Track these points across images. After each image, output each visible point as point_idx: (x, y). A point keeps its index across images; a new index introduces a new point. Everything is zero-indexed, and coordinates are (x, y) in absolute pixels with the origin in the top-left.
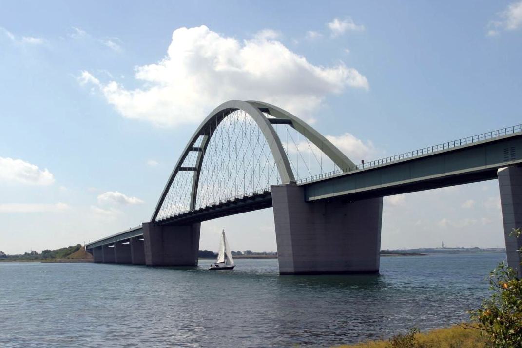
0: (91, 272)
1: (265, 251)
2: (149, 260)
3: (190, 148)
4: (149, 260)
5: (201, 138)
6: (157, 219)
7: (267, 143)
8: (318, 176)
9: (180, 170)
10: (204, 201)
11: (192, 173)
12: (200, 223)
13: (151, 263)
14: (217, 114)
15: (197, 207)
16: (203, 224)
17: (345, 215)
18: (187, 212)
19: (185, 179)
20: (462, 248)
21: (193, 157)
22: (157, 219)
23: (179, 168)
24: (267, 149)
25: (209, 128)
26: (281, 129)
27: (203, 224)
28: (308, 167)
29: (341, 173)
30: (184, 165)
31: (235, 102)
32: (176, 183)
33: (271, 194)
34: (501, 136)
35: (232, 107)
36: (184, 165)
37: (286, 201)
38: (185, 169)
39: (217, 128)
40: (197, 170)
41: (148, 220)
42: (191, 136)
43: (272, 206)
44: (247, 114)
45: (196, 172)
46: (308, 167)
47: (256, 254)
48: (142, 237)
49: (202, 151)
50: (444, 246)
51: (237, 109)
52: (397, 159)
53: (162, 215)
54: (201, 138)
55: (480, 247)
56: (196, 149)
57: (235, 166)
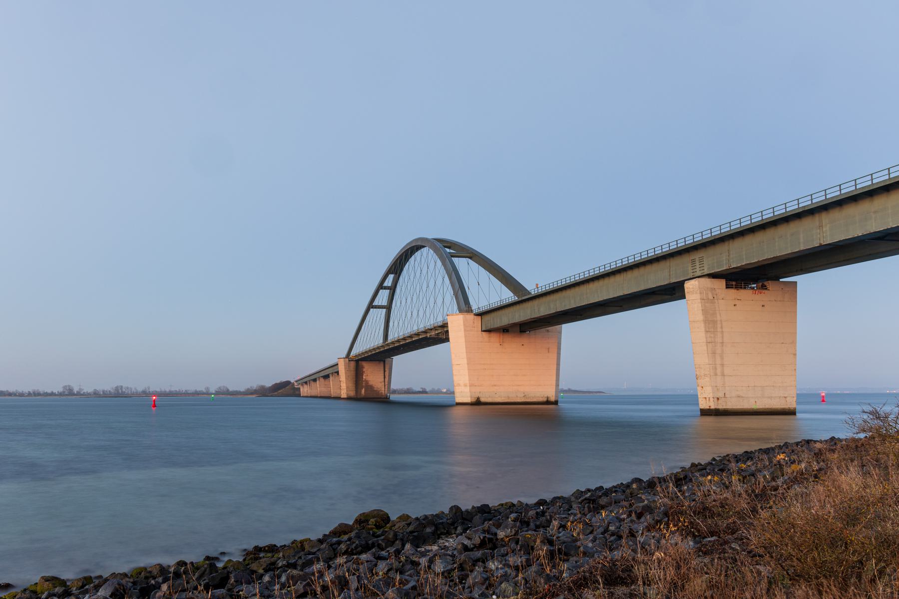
3: (381, 286)
5: (391, 277)
8: (510, 298)
9: (372, 308)
10: (397, 332)
11: (384, 310)
13: (345, 397)
14: (408, 250)
15: (391, 338)
17: (763, 306)
19: (377, 316)
21: (383, 296)
23: (371, 306)
25: (397, 267)
26: (462, 264)
30: (376, 303)
32: (368, 323)
33: (496, 528)
34: (696, 241)
35: (419, 243)
36: (376, 303)
39: (410, 260)
40: (389, 308)
42: (382, 275)
44: (430, 249)
45: (392, 291)
46: (500, 296)
49: (393, 289)
51: (424, 247)
53: (357, 350)
54: (391, 277)
56: (386, 288)
57: (426, 278)
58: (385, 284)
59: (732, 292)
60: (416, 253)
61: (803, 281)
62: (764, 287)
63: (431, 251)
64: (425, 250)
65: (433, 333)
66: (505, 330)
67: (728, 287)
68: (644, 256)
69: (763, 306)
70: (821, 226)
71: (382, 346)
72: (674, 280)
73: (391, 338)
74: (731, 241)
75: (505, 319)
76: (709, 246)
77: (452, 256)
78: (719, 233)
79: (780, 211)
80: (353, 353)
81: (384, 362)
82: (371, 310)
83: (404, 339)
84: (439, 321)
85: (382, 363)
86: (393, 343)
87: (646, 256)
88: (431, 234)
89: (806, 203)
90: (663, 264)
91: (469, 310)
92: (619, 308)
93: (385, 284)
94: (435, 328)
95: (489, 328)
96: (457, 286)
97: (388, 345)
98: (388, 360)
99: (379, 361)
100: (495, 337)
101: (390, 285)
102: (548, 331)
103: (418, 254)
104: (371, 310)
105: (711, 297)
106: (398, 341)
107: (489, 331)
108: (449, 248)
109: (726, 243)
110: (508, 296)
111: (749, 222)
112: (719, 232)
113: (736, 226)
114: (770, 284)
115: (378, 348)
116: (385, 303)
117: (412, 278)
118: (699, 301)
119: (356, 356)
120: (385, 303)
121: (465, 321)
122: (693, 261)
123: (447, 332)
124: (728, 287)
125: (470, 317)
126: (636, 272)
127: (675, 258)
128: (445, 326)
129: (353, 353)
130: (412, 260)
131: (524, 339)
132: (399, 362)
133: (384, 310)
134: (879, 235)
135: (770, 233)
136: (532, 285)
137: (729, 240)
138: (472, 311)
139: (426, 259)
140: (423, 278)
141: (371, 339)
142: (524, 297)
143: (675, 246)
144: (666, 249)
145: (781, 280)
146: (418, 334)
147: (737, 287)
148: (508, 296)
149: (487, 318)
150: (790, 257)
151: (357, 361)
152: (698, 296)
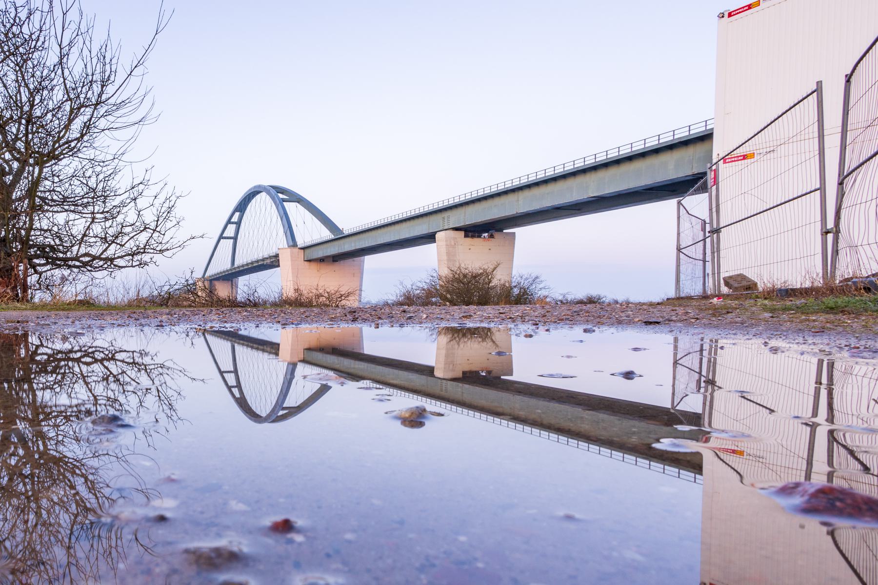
0: (508, 317)
3: (229, 222)
5: (237, 214)
10: (242, 259)
11: (232, 241)
14: (250, 194)
15: (236, 264)
17: (490, 249)
18: (228, 269)
19: (227, 244)
21: (231, 230)
23: (221, 237)
25: (242, 207)
26: (292, 208)
29: (332, 237)
31: (259, 186)
34: (622, 155)
37: (290, 260)
38: (225, 238)
40: (235, 238)
43: (707, 192)
49: (238, 224)
52: (366, 227)
54: (237, 214)
56: (233, 223)
58: (233, 220)
59: (469, 240)
60: (257, 196)
61: (518, 231)
62: (492, 236)
63: (268, 197)
64: (263, 194)
65: (268, 261)
66: (322, 260)
67: (466, 236)
68: (436, 207)
69: (490, 249)
70: (518, 200)
71: (231, 270)
72: (696, 171)
73: (236, 264)
74: (467, 206)
75: (320, 253)
76: (550, 182)
77: (284, 201)
78: (704, 129)
79: (541, 176)
80: (207, 274)
81: (232, 281)
82: (222, 240)
83: (247, 265)
84: (272, 252)
85: (230, 282)
86: (238, 267)
87: (458, 200)
88: (266, 183)
89: (580, 164)
90: (425, 219)
91: (295, 245)
92: (577, 212)
93: (233, 220)
94: (270, 257)
95: (309, 259)
96: (287, 226)
97: (235, 269)
98: (234, 280)
99: (228, 280)
100: (314, 266)
101: (236, 221)
102: (354, 260)
103: (258, 197)
104: (222, 240)
105: (453, 244)
106: (243, 266)
107: (309, 261)
108: (282, 193)
109: (464, 207)
110: (327, 234)
111: (544, 175)
112: (511, 185)
113: (501, 187)
114: (497, 235)
115: (227, 271)
116: (232, 235)
117: (258, 213)
118: (445, 246)
119: (210, 276)
120: (232, 235)
121: (292, 253)
122: (444, 218)
123: (279, 260)
124: (466, 236)
125: (296, 250)
126: (408, 224)
127: (532, 188)
128: (277, 256)
129: (207, 274)
130: (253, 201)
131: (337, 266)
132: (242, 281)
133: (232, 241)
134: (648, 187)
135: (490, 203)
136: (347, 226)
137: (518, 191)
138: (297, 246)
139: (263, 201)
140: (262, 216)
141: (222, 264)
142: (340, 236)
143: (482, 193)
144: (451, 202)
145: (504, 231)
146: (257, 261)
147: (473, 237)
148: (327, 234)
149: (307, 251)
150: (611, 195)
151: (211, 281)
152: (444, 243)
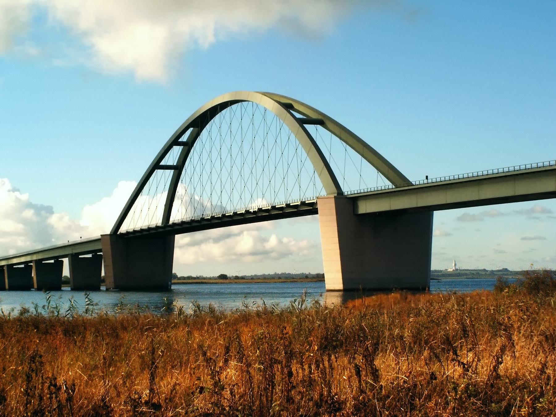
1: (213, 276)
2: (7, 287)
3: (175, 142)
4: (7, 287)
6: (171, 222)
7: (300, 146)
12: (432, 215)
16: (177, 237)
20: (485, 270)
22: (124, 229)
24: (303, 153)
27: (177, 237)
28: (269, 186)
40: (178, 169)
41: (108, 230)
45: (177, 171)
47: (184, 278)
48: (100, 250)
49: (188, 146)
50: (457, 267)
55: (510, 270)
